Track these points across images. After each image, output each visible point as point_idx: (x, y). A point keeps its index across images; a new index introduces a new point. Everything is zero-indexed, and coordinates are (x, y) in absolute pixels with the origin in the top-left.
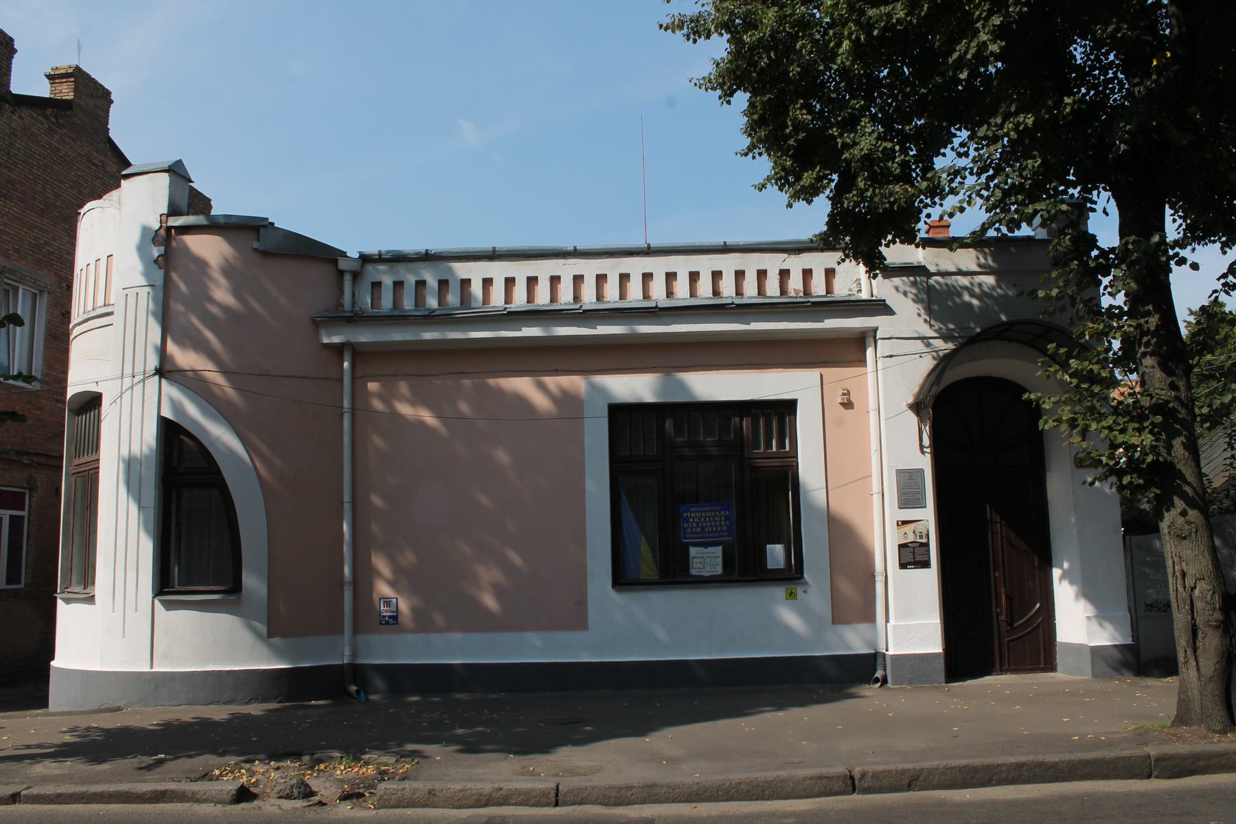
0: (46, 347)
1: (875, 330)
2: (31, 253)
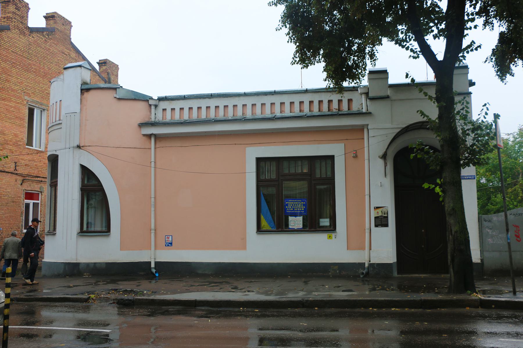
1: (368, 125)
2: (39, 94)
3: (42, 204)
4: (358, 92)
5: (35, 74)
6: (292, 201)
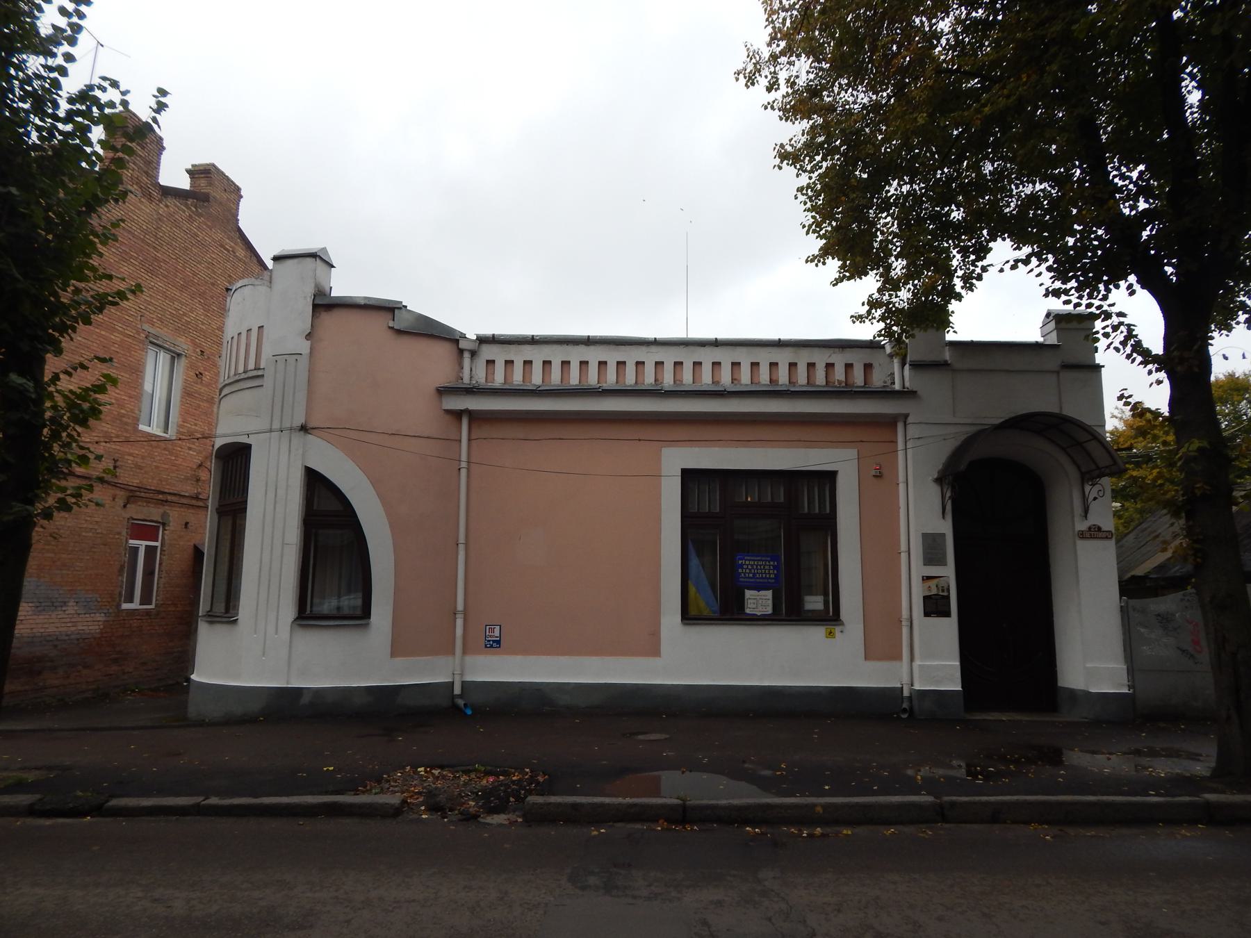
0: (182, 403)
1: (906, 416)
2: (171, 321)
3: (165, 549)
4: (885, 351)
5: (166, 280)
6: (752, 558)
